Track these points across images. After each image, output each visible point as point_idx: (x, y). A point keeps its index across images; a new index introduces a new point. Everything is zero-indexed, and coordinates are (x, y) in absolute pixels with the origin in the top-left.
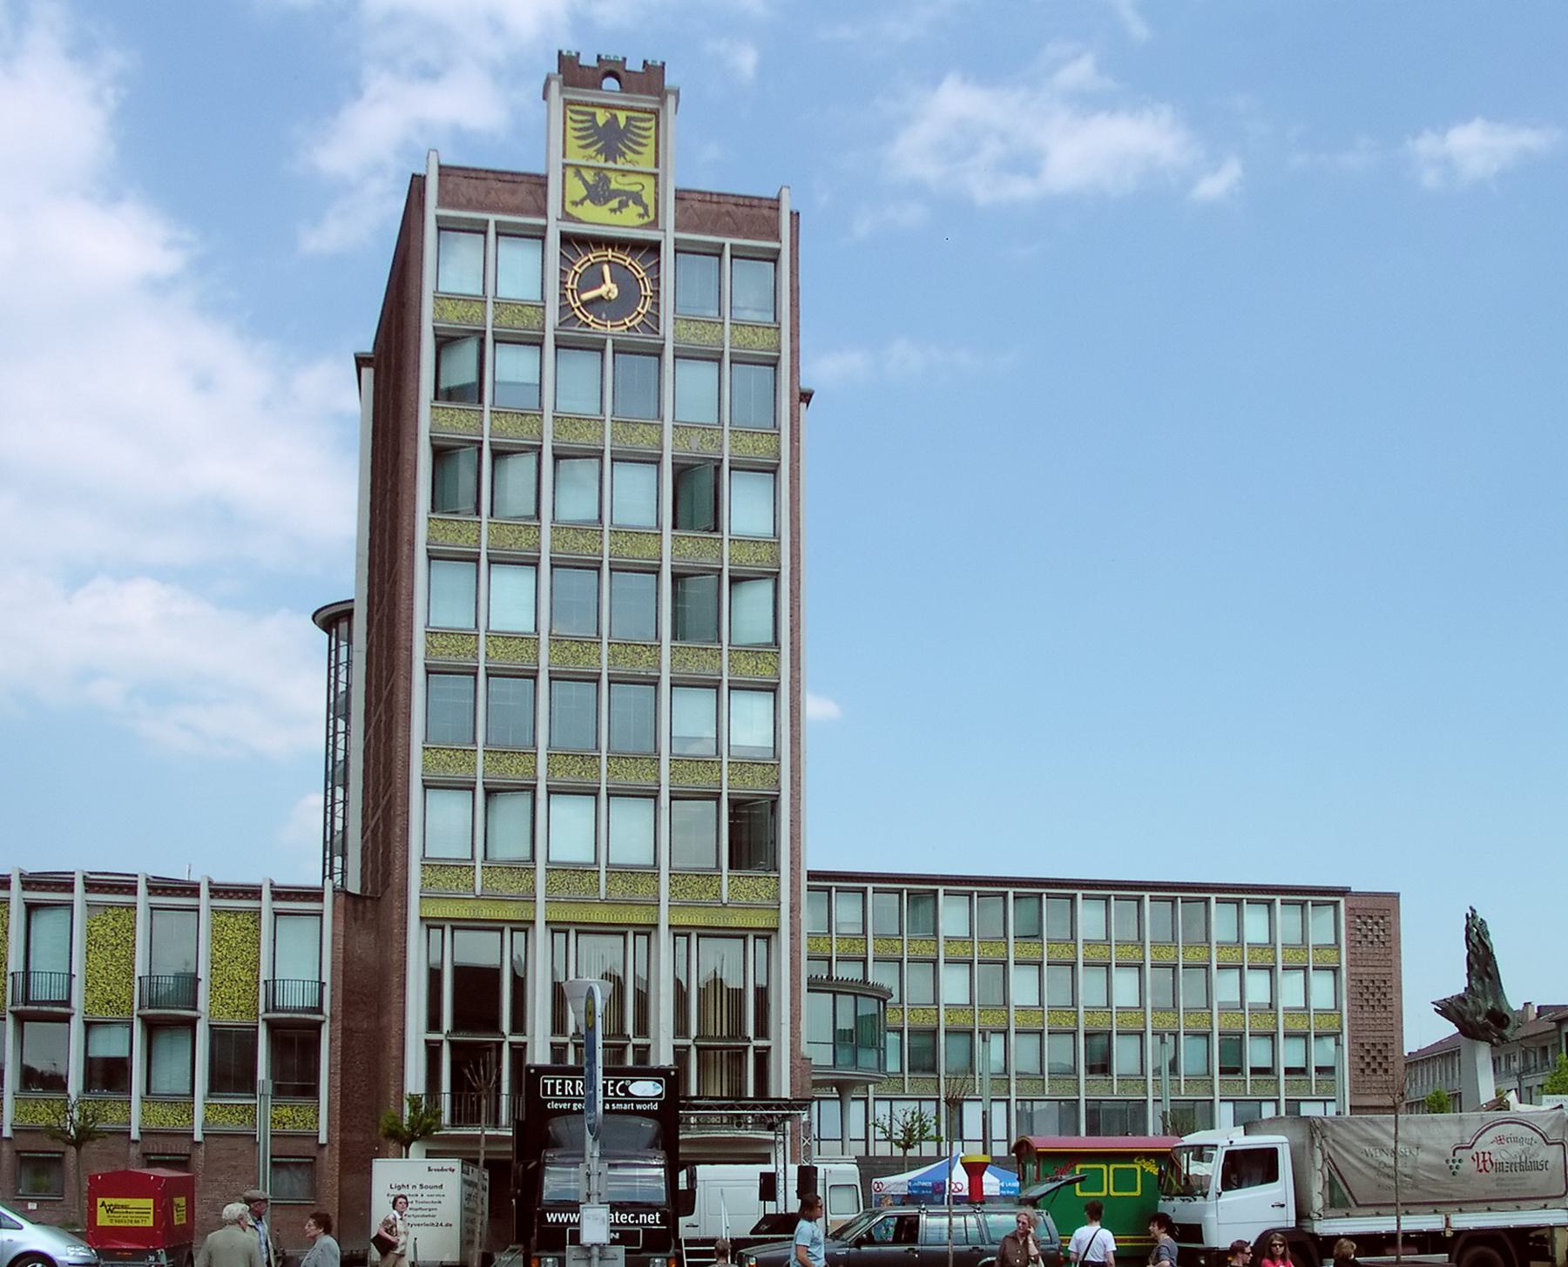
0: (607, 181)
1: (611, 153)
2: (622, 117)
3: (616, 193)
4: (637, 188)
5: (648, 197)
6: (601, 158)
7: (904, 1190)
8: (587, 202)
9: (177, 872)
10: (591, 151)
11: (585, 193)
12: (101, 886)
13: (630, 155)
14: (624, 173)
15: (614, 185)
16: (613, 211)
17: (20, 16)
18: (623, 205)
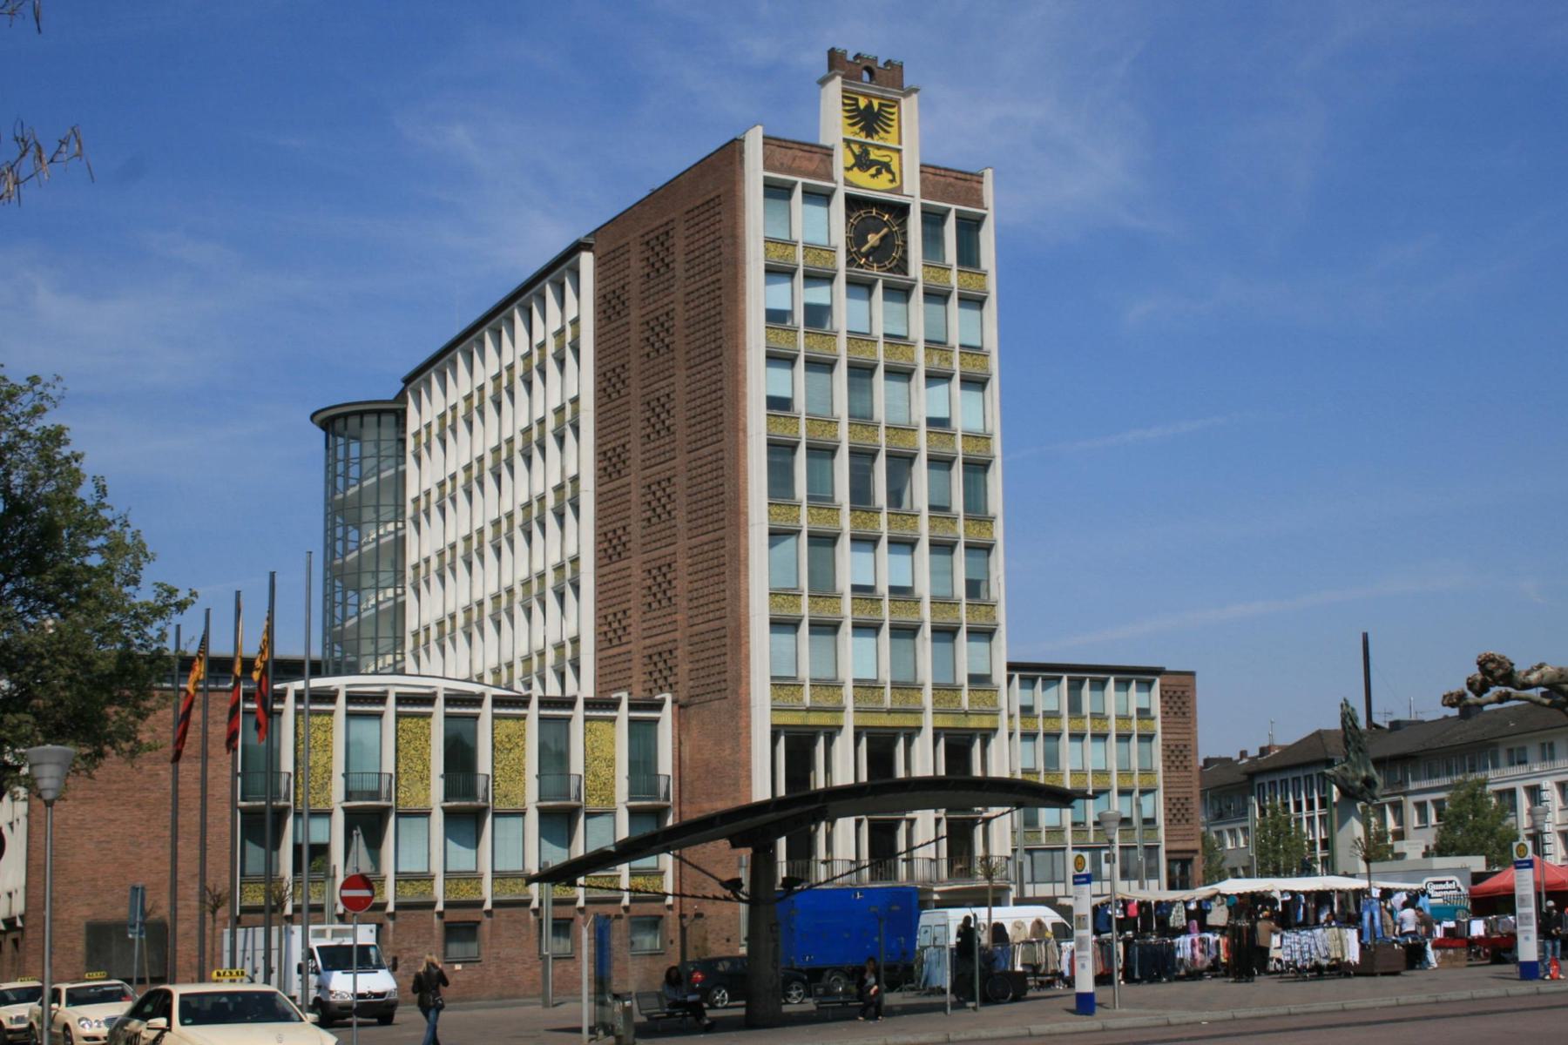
0: (867, 153)
1: (870, 131)
2: (876, 104)
4: (886, 159)
10: (856, 129)
11: (852, 161)
13: (882, 134)
14: (879, 147)
16: (873, 176)
18: (879, 172)
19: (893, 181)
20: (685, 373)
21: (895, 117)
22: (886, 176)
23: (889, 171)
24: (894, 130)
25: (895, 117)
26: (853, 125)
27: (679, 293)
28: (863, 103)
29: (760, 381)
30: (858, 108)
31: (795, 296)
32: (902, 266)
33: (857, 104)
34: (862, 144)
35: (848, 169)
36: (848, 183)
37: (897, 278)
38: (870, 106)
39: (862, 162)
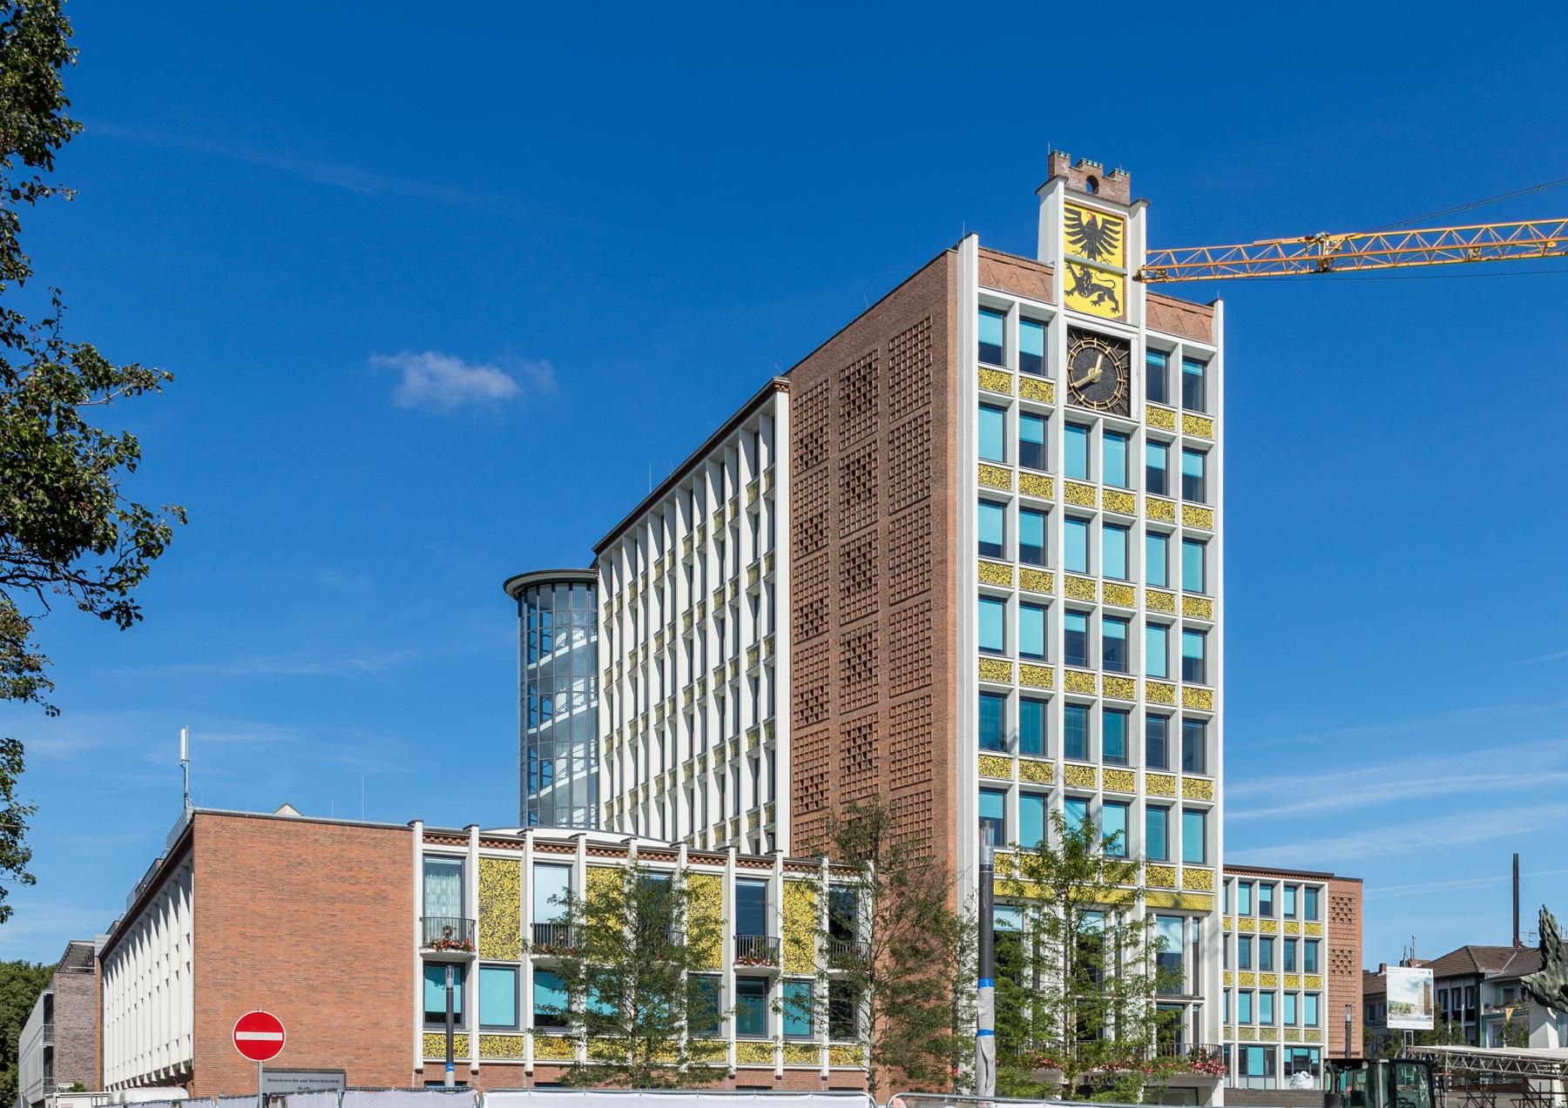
1: (1093, 252)
2: (1099, 218)
3: (1100, 288)
4: (1110, 285)
6: (1085, 254)
9: (432, 1095)
10: (1078, 247)
11: (1074, 284)
12: (501, 841)
13: (1105, 255)
14: (1102, 271)
15: (1094, 281)
16: (1095, 303)
17: (10, 631)
18: (1101, 298)
21: (1120, 236)
23: (1112, 298)
24: (1118, 252)
26: (1074, 242)
27: (884, 703)
28: (1085, 218)
29: (971, 625)
30: (1080, 225)
34: (1083, 266)
35: (1069, 293)
36: (1067, 307)
37: (1118, 420)
38: (1093, 221)
39: (1083, 286)
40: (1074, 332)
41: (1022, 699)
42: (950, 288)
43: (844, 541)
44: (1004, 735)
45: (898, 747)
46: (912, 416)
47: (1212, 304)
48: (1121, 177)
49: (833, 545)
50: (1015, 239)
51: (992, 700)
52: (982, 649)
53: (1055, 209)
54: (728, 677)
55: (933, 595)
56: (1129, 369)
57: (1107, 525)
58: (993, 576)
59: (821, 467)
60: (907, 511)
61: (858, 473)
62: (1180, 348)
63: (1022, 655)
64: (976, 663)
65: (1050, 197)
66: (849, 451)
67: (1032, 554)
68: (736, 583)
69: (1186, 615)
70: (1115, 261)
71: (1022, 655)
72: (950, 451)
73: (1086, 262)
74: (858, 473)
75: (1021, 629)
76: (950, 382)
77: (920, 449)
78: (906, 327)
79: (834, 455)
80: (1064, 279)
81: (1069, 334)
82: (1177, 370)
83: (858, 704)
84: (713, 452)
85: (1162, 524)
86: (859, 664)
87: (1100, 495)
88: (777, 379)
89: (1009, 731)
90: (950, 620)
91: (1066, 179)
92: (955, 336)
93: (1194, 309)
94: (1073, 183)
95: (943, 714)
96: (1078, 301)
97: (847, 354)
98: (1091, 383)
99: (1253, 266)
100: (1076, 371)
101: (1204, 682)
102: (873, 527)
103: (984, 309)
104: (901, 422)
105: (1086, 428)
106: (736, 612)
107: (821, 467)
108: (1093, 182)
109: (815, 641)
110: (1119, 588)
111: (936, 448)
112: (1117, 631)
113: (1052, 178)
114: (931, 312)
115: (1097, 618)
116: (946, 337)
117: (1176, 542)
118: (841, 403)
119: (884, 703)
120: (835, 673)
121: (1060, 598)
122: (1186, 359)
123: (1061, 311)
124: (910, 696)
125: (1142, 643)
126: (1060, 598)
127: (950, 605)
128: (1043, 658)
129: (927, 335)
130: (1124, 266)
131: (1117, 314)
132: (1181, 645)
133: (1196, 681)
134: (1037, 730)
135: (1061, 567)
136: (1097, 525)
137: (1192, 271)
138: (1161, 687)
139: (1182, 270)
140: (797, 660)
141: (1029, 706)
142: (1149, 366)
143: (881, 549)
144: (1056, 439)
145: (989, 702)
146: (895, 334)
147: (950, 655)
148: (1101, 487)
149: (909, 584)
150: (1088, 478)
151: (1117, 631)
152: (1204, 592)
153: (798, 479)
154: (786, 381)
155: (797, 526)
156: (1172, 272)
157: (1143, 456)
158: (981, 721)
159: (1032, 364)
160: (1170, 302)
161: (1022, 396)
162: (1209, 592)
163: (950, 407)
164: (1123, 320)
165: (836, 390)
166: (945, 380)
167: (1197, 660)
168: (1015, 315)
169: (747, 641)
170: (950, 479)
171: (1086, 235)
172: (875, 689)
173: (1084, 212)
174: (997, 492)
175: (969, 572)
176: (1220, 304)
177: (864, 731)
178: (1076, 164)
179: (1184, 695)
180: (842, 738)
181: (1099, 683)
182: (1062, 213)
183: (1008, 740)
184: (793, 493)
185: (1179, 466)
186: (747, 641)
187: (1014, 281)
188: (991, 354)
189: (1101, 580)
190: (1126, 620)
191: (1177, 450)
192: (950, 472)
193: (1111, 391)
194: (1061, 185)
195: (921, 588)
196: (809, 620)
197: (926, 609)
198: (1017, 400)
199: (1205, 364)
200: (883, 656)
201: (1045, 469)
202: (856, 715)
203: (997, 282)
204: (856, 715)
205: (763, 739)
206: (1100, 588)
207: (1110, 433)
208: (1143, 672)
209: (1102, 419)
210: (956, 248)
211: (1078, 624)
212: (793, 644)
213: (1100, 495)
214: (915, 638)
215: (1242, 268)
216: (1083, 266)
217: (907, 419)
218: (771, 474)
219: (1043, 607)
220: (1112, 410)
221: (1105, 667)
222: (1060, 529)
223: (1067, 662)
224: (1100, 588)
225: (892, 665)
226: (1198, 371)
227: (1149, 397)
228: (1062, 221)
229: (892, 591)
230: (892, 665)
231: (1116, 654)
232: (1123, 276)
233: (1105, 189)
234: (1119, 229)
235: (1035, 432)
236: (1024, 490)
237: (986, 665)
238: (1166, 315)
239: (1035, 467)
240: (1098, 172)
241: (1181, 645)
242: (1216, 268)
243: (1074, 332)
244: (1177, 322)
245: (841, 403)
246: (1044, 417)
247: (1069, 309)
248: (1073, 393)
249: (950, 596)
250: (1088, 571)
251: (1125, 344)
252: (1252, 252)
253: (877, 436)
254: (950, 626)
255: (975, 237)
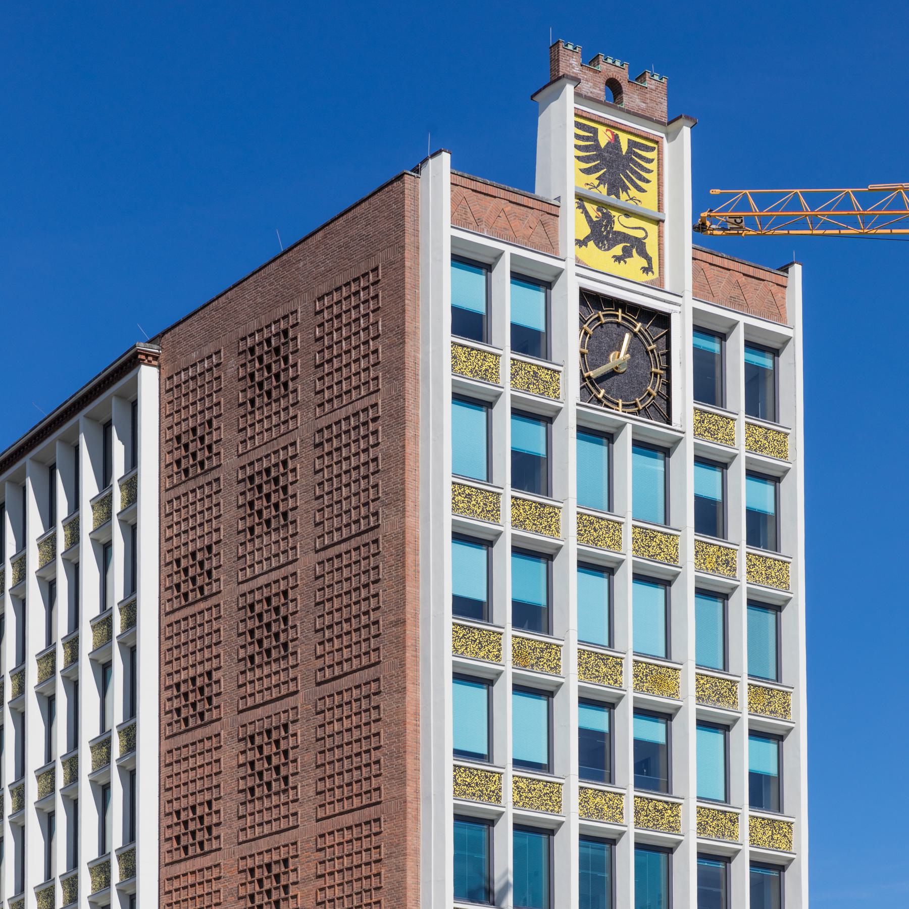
0: (610, 220)
1: (615, 187)
2: (624, 139)
3: (625, 237)
4: (640, 234)
5: (651, 248)
6: (603, 189)
7: (43, 554)
8: (591, 244)
9: (185, 743)
10: (593, 178)
11: (587, 231)
13: (633, 192)
14: (628, 214)
15: (617, 227)
16: (618, 259)
18: (627, 253)
19: (647, 270)
20: (296, 437)
21: (653, 166)
22: (637, 262)
23: (643, 253)
24: (651, 188)
25: (652, 177)
26: (587, 171)
27: (307, 830)
28: (604, 137)
29: (441, 717)
30: (597, 146)
31: (470, 290)
32: (663, 410)
33: (595, 138)
34: (601, 205)
35: (581, 243)
36: (579, 264)
37: (654, 427)
38: (615, 143)
39: (601, 234)
40: (589, 299)
41: (518, 827)
42: (409, 226)
43: (245, 588)
44: (490, 880)
45: (329, 894)
46: (350, 410)
47: (785, 269)
48: (654, 83)
49: (228, 591)
50: (503, 164)
51: (473, 827)
52: (458, 753)
53: (560, 123)
54: (60, 783)
55: (384, 671)
56: (668, 355)
57: (639, 578)
58: (473, 646)
59: (209, 478)
60: (343, 547)
61: (266, 490)
62: (740, 329)
63: (517, 763)
64: (449, 774)
65: (554, 105)
66: (253, 456)
67: (531, 616)
68: (73, 643)
69: (753, 711)
70: (647, 202)
71: (517, 763)
72: (410, 462)
73: (604, 205)
74: (266, 490)
75: (515, 726)
76: (409, 362)
77: (363, 458)
78: (340, 280)
79: (229, 463)
80: (573, 224)
81: (582, 302)
82: (736, 360)
83: (266, 829)
84: (42, 446)
85: (718, 579)
86: (268, 765)
87: (628, 534)
88: (141, 346)
89: (497, 874)
90: (410, 709)
91: (576, 81)
92: (416, 297)
93: (761, 274)
94: (586, 87)
95: (400, 848)
96: (593, 254)
97: (248, 314)
98: (613, 373)
99: (866, 220)
100: (592, 354)
101: (779, 809)
102: (290, 569)
103: (458, 260)
104: (334, 417)
105: (608, 437)
106: (74, 688)
107: (209, 478)
108: (614, 86)
109: (199, 734)
110: (657, 670)
111: (387, 457)
112: (654, 732)
113: (556, 79)
114: (379, 260)
115: (625, 712)
116: (402, 297)
117: (738, 605)
118: (241, 385)
119: (307, 830)
120: (230, 781)
121: (572, 681)
122: (750, 346)
123: (570, 268)
124: (348, 820)
125: (690, 750)
126: (572, 681)
127: (410, 686)
128: (547, 768)
129: (375, 293)
130: (660, 207)
131: (651, 277)
132: (746, 756)
133: (768, 809)
134: (537, 874)
135: (573, 637)
136: (624, 577)
137: (780, 222)
138: (716, 817)
139: (764, 220)
140: (169, 760)
141: (528, 837)
142: (698, 353)
143: (302, 600)
144: (565, 451)
145: (468, 830)
146: (324, 289)
147: (409, 759)
148: (629, 522)
149: (346, 653)
150: (610, 508)
151: (654, 732)
152: (778, 678)
153: (172, 494)
154: (154, 349)
155: (171, 563)
156: (751, 222)
157: (688, 481)
158: (457, 859)
159: (528, 341)
160: (726, 263)
161: (514, 386)
162: (785, 680)
163: (409, 397)
164: (658, 285)
165: (232, 366)
166: (401, 359)
167: (768, 777)
168: (503, 271)
169: (90, 730)
170: (409, 505)
171: (608, 163)
172: (293, 808)
173: (601, 129)
174: (479, 524)
175: (437, 640)
176: (797, 271)
177: (275, 870)
178: (591, 61)
179: (752, 828)
180: (242, 878)
181: (629, 805)
182: (572, 130)
183: (497, 887)
184: (164, 515)
185: (742, 494)
186: (90, 730)
187: (502, 221)
188: (470, 324)
189: (630, 658)
190: (666, 717)
191: (738, 472)
192: (409, 494)
193: (642, 384)
194: (569, 89)
195: (365, 661)
196: (188, 703)
197: (372, 692)
198: (508, 392)
199: (776, 353)
200: (305, 758)
201: (548, 493)
202: (263, 845)
203: (478, 222)
204: (263, 845)
205: (116, 876)
206: (628, 669)
207: (641, 446)
208: (693, 793)
209: (630, 426)
210: (417, 170)
211: (598, 720)
212: (164, 737)
213: (628, 534)
214: (356, 734)
215: (852, 221)
216: (601, 205)
217: (343, 413)
218: (131, 485)
219: (547, 694)
220: (645, 412)
221: (638, 785)
222: (570, 581)
223: (583, 775)
224: (628, 669)
225: (319, 773)
226: (766, 362)
227: (698, 397)
228: (571, 141)
229: (319, 663)
230: (319, 773)
231: (653, 766)
232: (659, 222)
233: (631, 98)
234: (652, 155)
235: (533, 439)
236: (517, 523)
237: (464, 777)
238: (721, 281)
239: (533, 490)
240: (622, 75)
241: (746, 756)
242: (815, 221)
243: (589, 299)
244: (736, 292)
245: (241, 385)
246: (546, 419)
247: (583, 266)
248: (589, 385)
249: (410, 673)
250: (611, 644)
251: (663, 320)
252: (866, 199)
253: (296, 437)
254: (410, 719)
255: (446, 157)
